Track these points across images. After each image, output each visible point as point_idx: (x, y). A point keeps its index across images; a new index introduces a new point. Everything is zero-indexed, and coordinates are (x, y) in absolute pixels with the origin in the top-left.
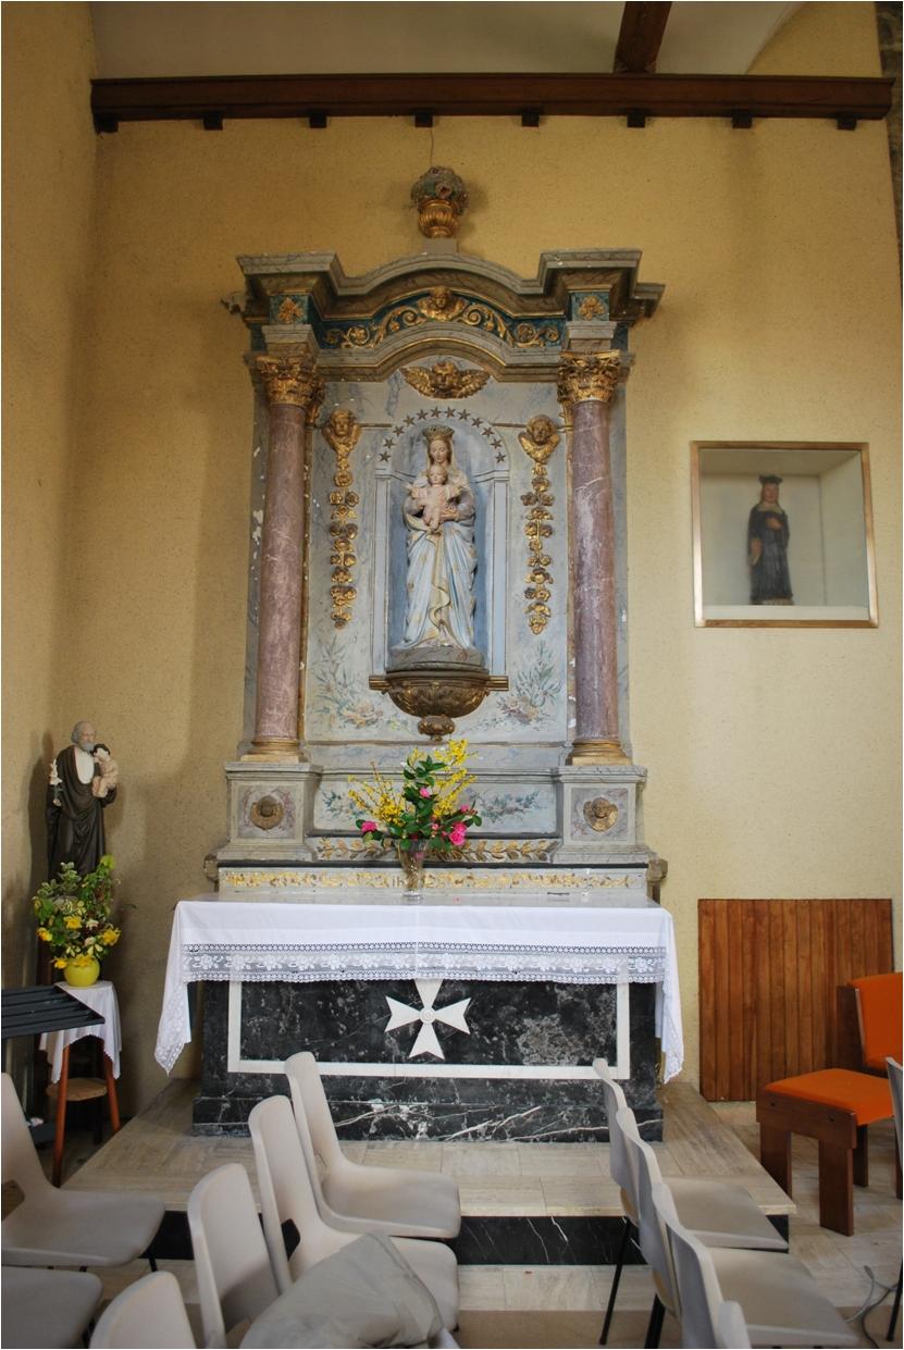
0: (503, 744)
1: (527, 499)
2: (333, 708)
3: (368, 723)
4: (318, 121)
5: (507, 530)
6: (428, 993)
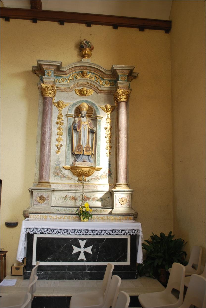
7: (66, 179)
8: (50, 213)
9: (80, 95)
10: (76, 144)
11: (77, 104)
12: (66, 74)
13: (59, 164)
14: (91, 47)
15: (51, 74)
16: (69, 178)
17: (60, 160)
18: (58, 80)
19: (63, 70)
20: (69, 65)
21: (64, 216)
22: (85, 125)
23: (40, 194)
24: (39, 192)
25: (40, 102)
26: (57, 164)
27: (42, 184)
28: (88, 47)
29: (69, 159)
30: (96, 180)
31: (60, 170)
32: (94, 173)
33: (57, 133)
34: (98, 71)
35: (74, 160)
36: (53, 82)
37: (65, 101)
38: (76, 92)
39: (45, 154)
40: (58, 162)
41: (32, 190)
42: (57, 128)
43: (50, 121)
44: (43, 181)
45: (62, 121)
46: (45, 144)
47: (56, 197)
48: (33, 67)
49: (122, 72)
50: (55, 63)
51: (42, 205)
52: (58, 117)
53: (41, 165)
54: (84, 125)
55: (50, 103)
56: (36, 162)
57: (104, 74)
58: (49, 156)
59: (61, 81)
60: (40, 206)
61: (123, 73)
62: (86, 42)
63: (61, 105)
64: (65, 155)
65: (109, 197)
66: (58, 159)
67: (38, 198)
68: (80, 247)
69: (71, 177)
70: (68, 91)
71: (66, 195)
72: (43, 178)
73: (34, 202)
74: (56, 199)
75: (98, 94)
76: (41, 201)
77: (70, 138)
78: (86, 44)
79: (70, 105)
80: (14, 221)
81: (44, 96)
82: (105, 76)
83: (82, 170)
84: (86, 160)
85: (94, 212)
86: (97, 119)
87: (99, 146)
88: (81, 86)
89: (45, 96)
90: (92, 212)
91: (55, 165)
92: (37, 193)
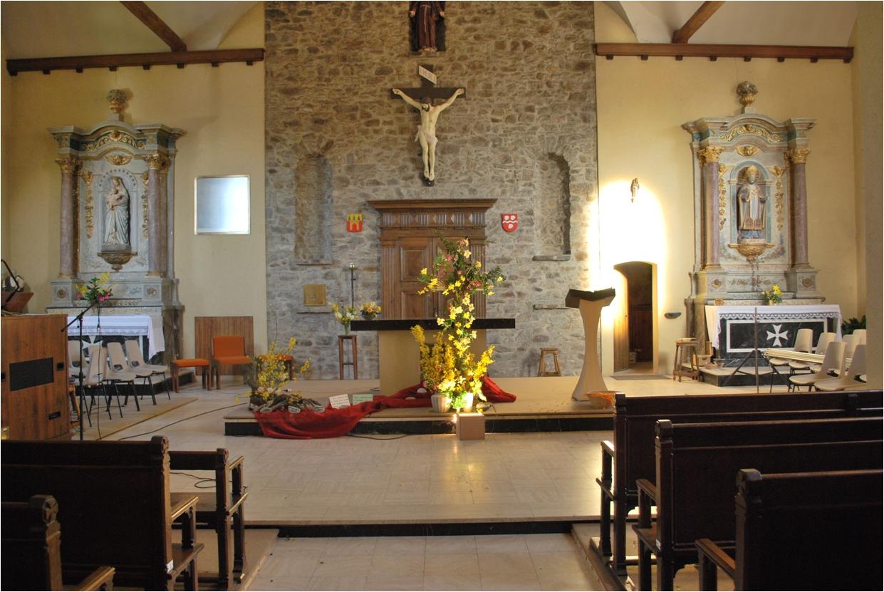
0: (136, 272)
1: (143, 197)
2: (88, 263)
3: (98, 267)
4: (79, 70)
5: (137, 207)
6: (92, 339)
7: (731, 260)
16: (735, 259)
62: (750, 86)
68: (774, 333)
76: (716, 286)
82: (774, 129)
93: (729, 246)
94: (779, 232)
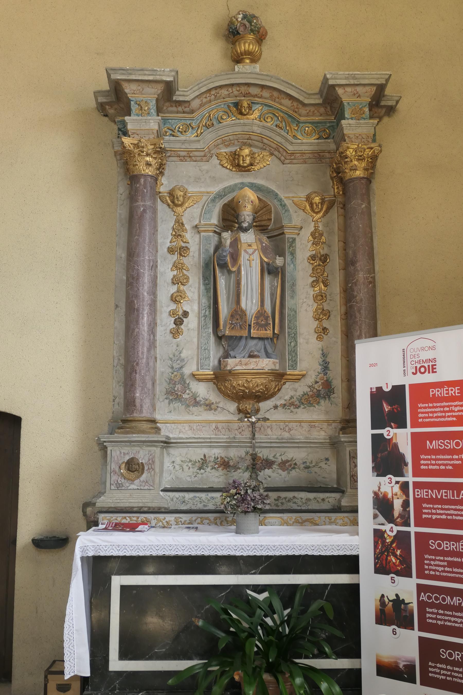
7: (201, 409)
8: (160, 508)
9: (234, 169)
10: (228, 310)
11: (225, 195)
12: (192, 112)
13: (182, 367)
14: (258, 32)
15: (149, 109)
16: (209, 406)
17: (183, 355)
18: (168, 129)
19: (181, 99)
20: (198, 84)
21: (201, 518)
22: (250, 251)
23: (128, 454)
24: (126, 450)
25: (121, 194)
26: (176, 366)
27: (133, 424)
28: (252, 31)
29: (209, 351)
30: (289, 411)
31: (185, 382)
32: (283, 391)
33: (172, 279)
34: (283, 96)
35: (224, 353)
36: (155, 132)
37: (191, 189)
38: (221, 161)
39: (140, 338)
40: (178, 362)
41: (105, 444)
42: (170, 266)
43: (150, 242)
44: (136, 415)
45: (183, 245)
46: (138, 310)
47: (173, 462)
48: (97, 94)
49: (354, 94)
50: (160, 75)
51: (136, 487)
52: (174, 233)
53: (129, 371)
54: (247, 253)
55: (149, 192)
56: (115, 365)
57: (300, 106)
58: (152, 345)
59: (179, 131)
60: (129, 488)
61: (357, 95)
62: (245, 17)
63: (181, 199)
64: (195, 340)
65: (327, 459)
66: (177, 353)
67: (123, 466)
69: (216, 403)
70: (200, 158)
71: (205, 456)
72: (135, 406)
73: (113, 479)
74: (174, 467)
75: (283, 164)
76: (132, 475)
77: (210, 292)
78: (245, 22)
79: (205, 198)
80: (59, 532)
81: (131, 174)
82: (303, 111)
83: (247, 380)
84: (258, 351)
85: (289, 504)
86: (283, 233)
87: (293, 313)
88: (234, 144)
89: (133, 172)
90: (282, 503)
91: (170, 370)
92: (121, 453)
93: (193, 375)
94: (320, 345)
